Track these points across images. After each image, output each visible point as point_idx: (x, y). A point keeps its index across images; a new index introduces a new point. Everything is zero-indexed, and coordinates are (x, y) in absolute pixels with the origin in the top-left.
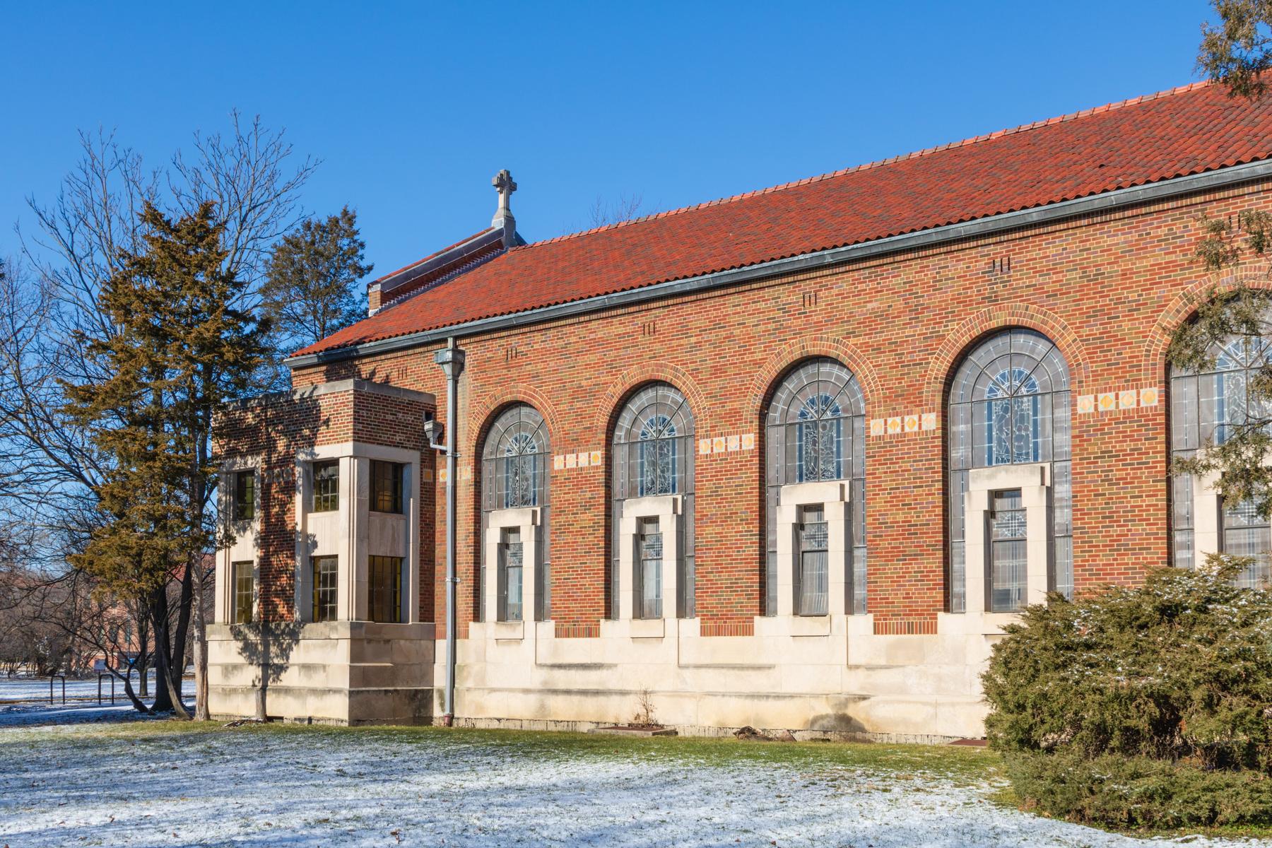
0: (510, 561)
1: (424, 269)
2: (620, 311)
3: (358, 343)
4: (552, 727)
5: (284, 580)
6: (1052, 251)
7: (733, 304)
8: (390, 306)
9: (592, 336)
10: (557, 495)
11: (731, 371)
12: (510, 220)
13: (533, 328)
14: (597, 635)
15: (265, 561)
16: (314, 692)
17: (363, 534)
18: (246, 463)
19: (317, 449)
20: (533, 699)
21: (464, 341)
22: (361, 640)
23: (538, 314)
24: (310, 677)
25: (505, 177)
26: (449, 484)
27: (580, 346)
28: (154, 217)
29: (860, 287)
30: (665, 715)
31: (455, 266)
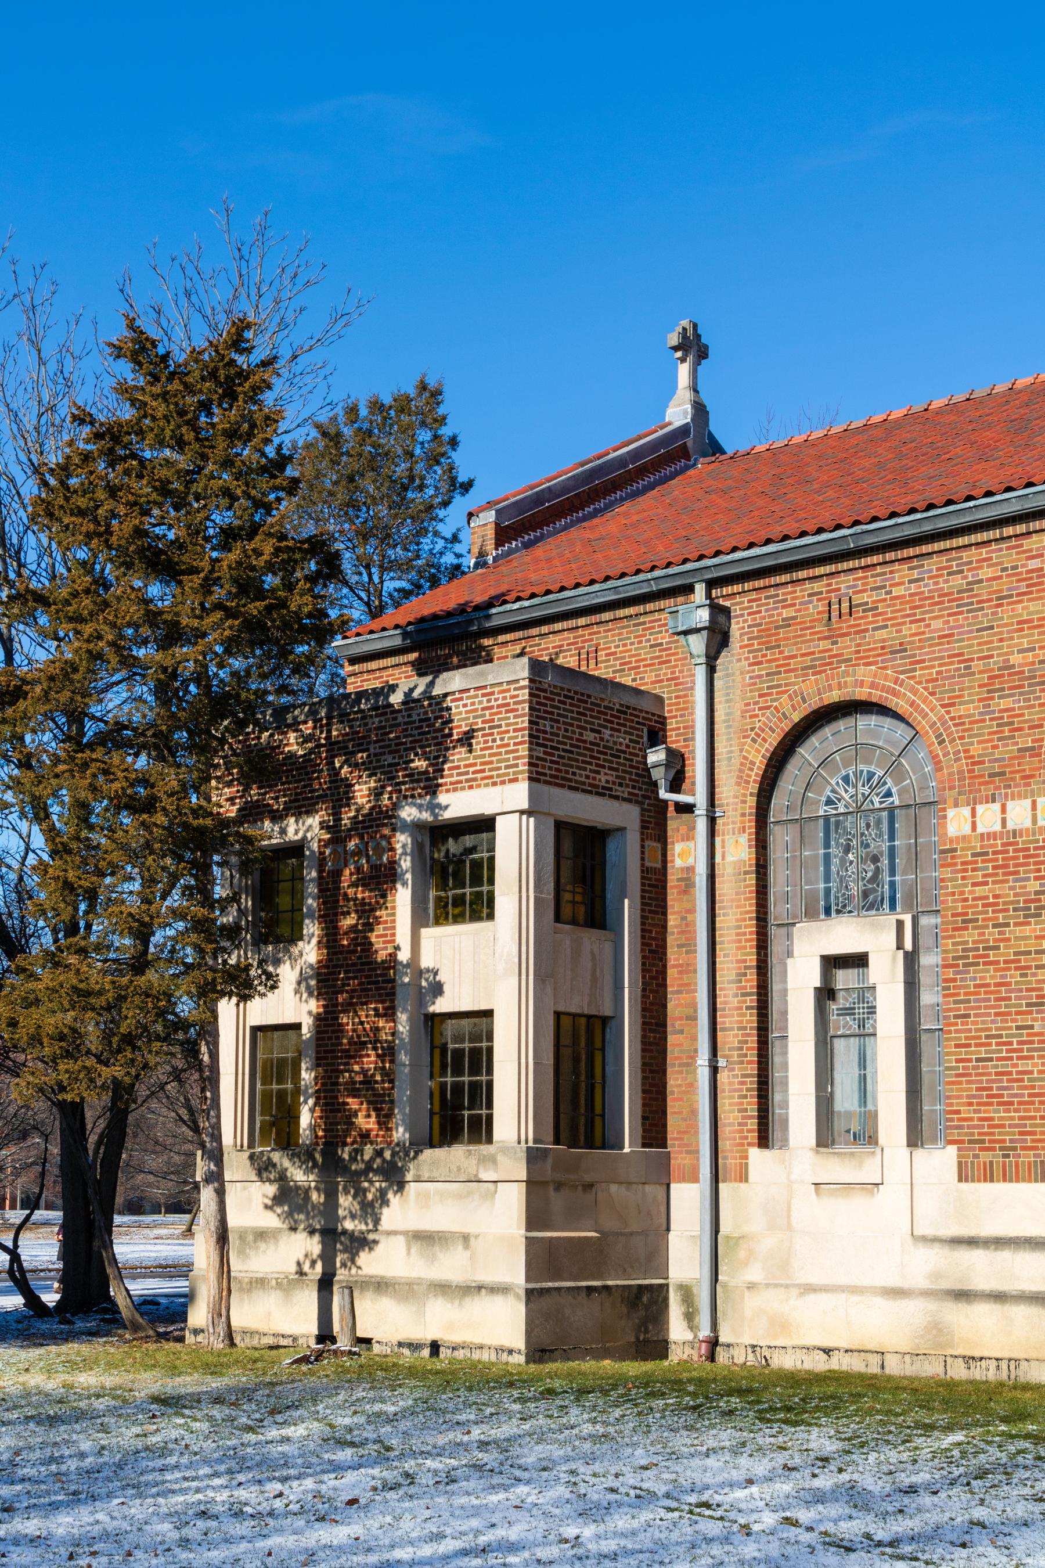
0: (839, 1024)
1: (564, 488)
3: (490, 604)
4: (959, 1372)
5: (370, 1060)
8: (511, 552)
9: (1033, 564)
10: (957, 889)
12: (700, 410)
13: (890, 556)
15: (326, 1023)
16: (442, 1288)
17: (546, 969)
18: (283, 832)
19: (443, 798)
21: (729, 590)
22: (545, 1183)
23: (907, 525)
24: (433, 1259)
25: (690, 333)
26: (702, 869)
27: (1004, 585)
28: (140, 349)
31: (614, 486)
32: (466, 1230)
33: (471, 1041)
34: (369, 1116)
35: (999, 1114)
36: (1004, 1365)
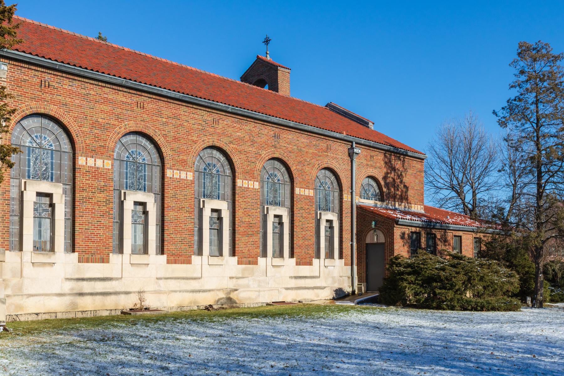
2: (125, 90)
6: (290, 137)
7: (183, 110)
9: (106, 96)
11: (182, 141)
20: (67, 300)
29: (235, 125)
30: (152, 302)
35: (91, 244)
36: (92, 312)
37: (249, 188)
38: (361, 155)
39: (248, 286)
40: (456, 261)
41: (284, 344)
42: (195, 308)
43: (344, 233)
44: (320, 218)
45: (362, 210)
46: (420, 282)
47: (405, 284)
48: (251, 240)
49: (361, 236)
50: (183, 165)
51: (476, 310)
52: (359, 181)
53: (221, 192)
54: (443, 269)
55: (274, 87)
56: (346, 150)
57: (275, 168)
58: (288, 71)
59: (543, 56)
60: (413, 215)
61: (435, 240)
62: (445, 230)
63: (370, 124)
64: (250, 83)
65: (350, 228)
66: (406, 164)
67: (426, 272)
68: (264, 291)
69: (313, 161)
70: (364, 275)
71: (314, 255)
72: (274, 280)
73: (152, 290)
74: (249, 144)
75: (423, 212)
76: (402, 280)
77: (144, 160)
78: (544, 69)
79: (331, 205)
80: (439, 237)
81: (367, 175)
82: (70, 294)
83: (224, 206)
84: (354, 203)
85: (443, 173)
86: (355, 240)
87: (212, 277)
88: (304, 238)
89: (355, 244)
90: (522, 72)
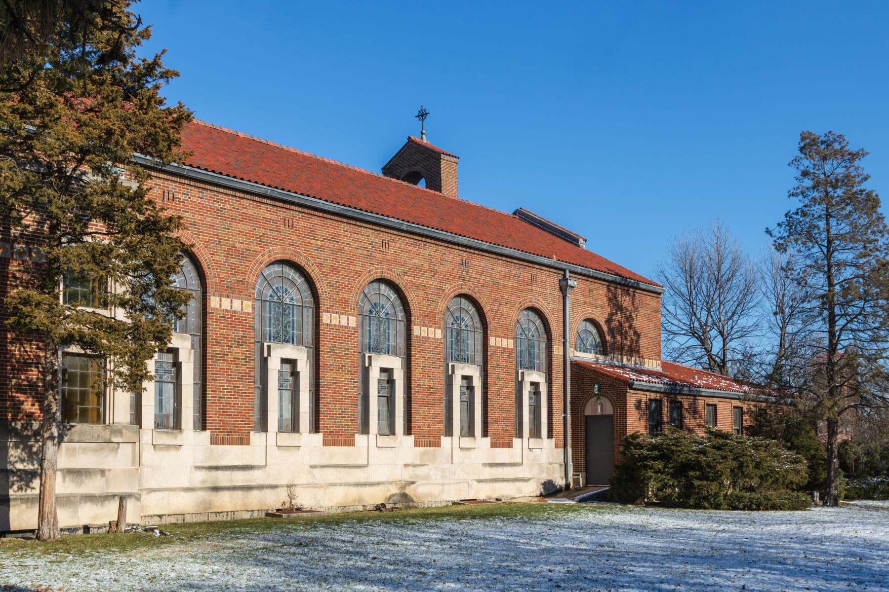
2: (269, 202)
6: (482, 264)
7: (343, 229)
9: (244, 211)
13: (193, 183)
14: (248, 443)
16: (90, 498)
20: (202, 495)
27: (234, 214)
29: (410, 248)
30: (306, 499)
32: (102, 467)
33: (81, 369)
34: (33, 405)
37: (428, 338)
38: (576, 289)
39: (428, 477)
40: (721, 441)
41: (535, 548)
42: (361, 508)
43: (554, 401)
44: (523, 379)
45: (577, 366)
46: (671, 471)
47: (650, 474)
48: (432, 411)
49: (577, 404)
50: (343, 306)
51: (750, 508)
52: (574, 326)
53: (392, 343)
54: (703, 452)
55: (435, 183)
56: (557, 282)
57: (461, 309)
58: (454, 160)
59: (836, 153)
60: (649, 375)
61: (681, 411)
62: (695, 396)
63: (581, 241)
64: (398, 179)
65: (562, 394)
66: (637, 301)
67: (679, 456)
68: (450, 484)
69: (513, 298)
70: (582, 461)
71: (514, 432)
72: (465, 469)
73: (305, 482)
74: (429, 275)
75: (660, 369)
76: (646, 467)
77: (292, 299)
78: (837, 171)
79: (536, 361)
80: (686, 407)
81: (584, 317)
82: (201, 489)
83: (395, 363)
84: (568, 358)
85: (679, 311)
86: (569, 411)
87: (382, 464)
88: (501, 409)
89: (569, 416)
90: (805, 174)
